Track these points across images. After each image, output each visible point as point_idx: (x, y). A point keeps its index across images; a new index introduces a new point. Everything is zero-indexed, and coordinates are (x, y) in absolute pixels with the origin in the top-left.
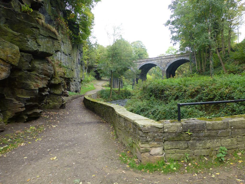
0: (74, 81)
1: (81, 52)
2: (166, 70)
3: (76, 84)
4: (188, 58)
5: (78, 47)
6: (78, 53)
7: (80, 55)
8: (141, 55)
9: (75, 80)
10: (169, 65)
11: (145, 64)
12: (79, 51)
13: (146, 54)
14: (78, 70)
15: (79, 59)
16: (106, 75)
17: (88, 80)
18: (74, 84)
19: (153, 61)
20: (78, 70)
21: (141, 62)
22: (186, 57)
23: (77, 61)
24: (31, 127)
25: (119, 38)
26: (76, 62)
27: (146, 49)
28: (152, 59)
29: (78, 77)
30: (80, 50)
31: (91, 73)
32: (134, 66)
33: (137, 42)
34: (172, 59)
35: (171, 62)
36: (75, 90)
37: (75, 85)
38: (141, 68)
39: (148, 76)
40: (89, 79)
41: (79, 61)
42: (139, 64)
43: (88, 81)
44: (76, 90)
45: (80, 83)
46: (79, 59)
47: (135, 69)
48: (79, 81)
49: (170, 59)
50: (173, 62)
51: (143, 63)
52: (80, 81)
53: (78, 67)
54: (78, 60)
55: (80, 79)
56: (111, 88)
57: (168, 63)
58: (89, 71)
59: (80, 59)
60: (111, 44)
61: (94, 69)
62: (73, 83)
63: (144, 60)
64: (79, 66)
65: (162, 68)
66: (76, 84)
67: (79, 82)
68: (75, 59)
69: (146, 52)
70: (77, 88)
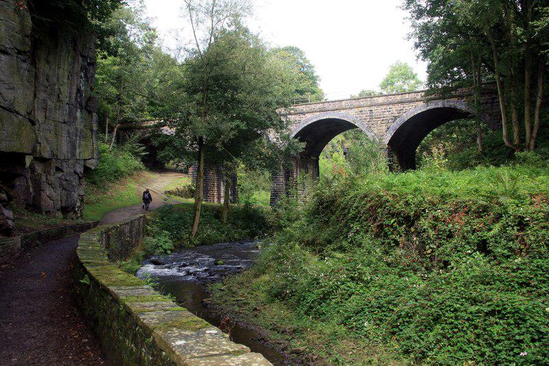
0: (58, 169)
1: (89, 64)
2: (386, 140)
3: (64, 183)
4: (461, 105)
5: (75, 45)
6: (77, 67)
7: (86, 76)
8: (305, 88)
9: (59, 166)
10: (396, 125)
11: (314, 120)
12: (81, 58)
13: (313, 92)
14: (72, 130)
15: (79, 90)
16: (180, 153)
17: (116, 172)
18: (57, 184)
19: (342, 112)
20: (72, 130)
21: (303, 113)
22: (455, 99)
23: (70, 97)
24: (330, 166)
25: (225, 24)
26: (67, 100)
27: (315, 75)
28: (339, 105)
29: (74, 155)
30: (82, 56)
31: (128, 146)
32: (280, 126)
33: (286, 49)
34: (407, 106)
35: (406, 117)
36: (59, 206)
37: (61, 185)
38: (304, 134)
39: (323, 162)
40: (121, 164)
41: (81, 96)
42: (301, 118)
43: (118, 175)
44: (64, 205)
45: (80, 178)
46: (79, 90)
47: (284, 138)
48: (75, 172)
49: (399, 107)
50: (412, 115)
51: (308, 116)
52: (82, 170)
53: (75, 118)
54: (75, 91)
55: (82, 162)
56: (198, 200)
57: (395, 118)
58: (120, 141)
59: (86, 91)
60: (203, 48)
61: (139, 134)
62: (52, 178)
63: (313, 106)
64: (78, 114)
65: (373, 136)
66: (64, 183)
67: (76, 176)
68: (65, 90)
69: (314, 84)
70: (69, 196)
